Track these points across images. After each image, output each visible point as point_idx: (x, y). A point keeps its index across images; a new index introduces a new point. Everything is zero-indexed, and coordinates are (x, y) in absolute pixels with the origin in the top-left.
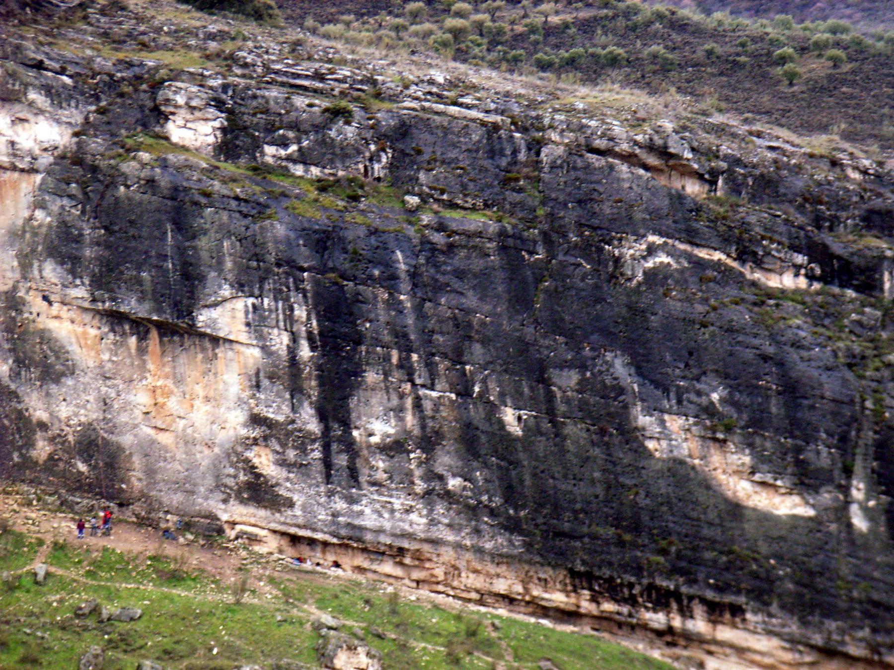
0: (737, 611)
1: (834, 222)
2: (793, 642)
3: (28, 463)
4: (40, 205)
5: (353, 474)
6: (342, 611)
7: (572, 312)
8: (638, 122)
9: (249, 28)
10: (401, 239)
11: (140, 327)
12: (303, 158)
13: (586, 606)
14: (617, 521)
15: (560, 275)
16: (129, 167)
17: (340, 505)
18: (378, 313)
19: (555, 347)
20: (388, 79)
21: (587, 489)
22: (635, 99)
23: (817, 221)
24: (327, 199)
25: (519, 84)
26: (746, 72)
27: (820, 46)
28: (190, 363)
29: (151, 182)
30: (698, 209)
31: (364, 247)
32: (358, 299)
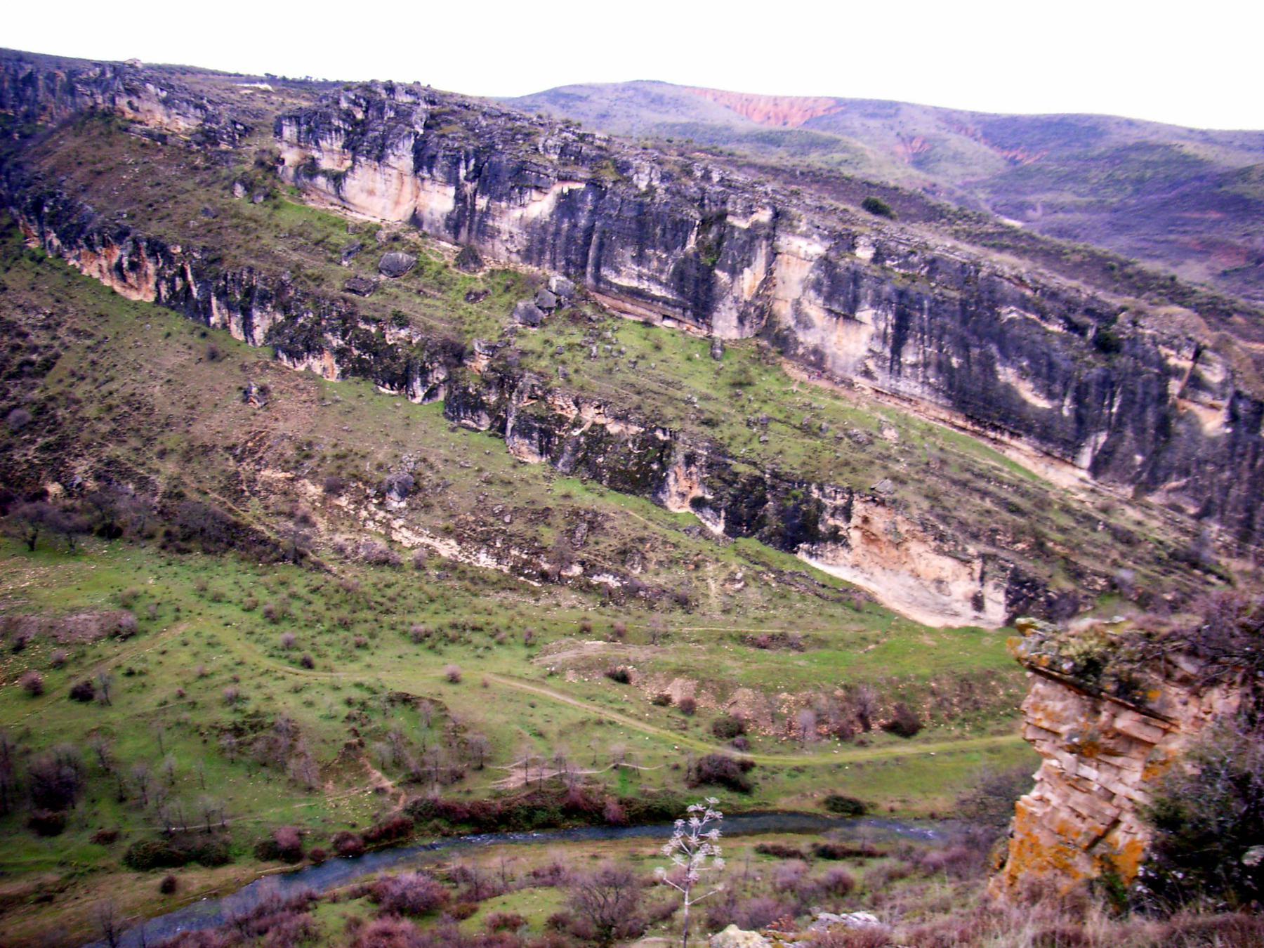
0: (1019, 436)
1: (1075, 311)
2: (1036, 449)
3: (795, 355)
4: (811, 272)
5: (899, 373)
6: (889, 417)
7: (980, 329)
8: (1013, 268)
9: (888, 222)
10: (927, 297)
11: (838, 315)
12: (899, 266)
13: (969, 426)
14: (984, 400)
15: (979, 315)
16: (842, 263)
17: (893, 382)
18: (915, 322)
19: (973, 340)
20: (931, 243)
21: (976, 388)
22: (1013, 260)
23: (1069, 309)
24: (905, 281)
25: (975, 250)
26: (1053, 256)
27: (1080, 251)
28: (852, 328)
29: (848, 269)
30: (1029, 300)
31: (915, 297)
32: (909, 315)
